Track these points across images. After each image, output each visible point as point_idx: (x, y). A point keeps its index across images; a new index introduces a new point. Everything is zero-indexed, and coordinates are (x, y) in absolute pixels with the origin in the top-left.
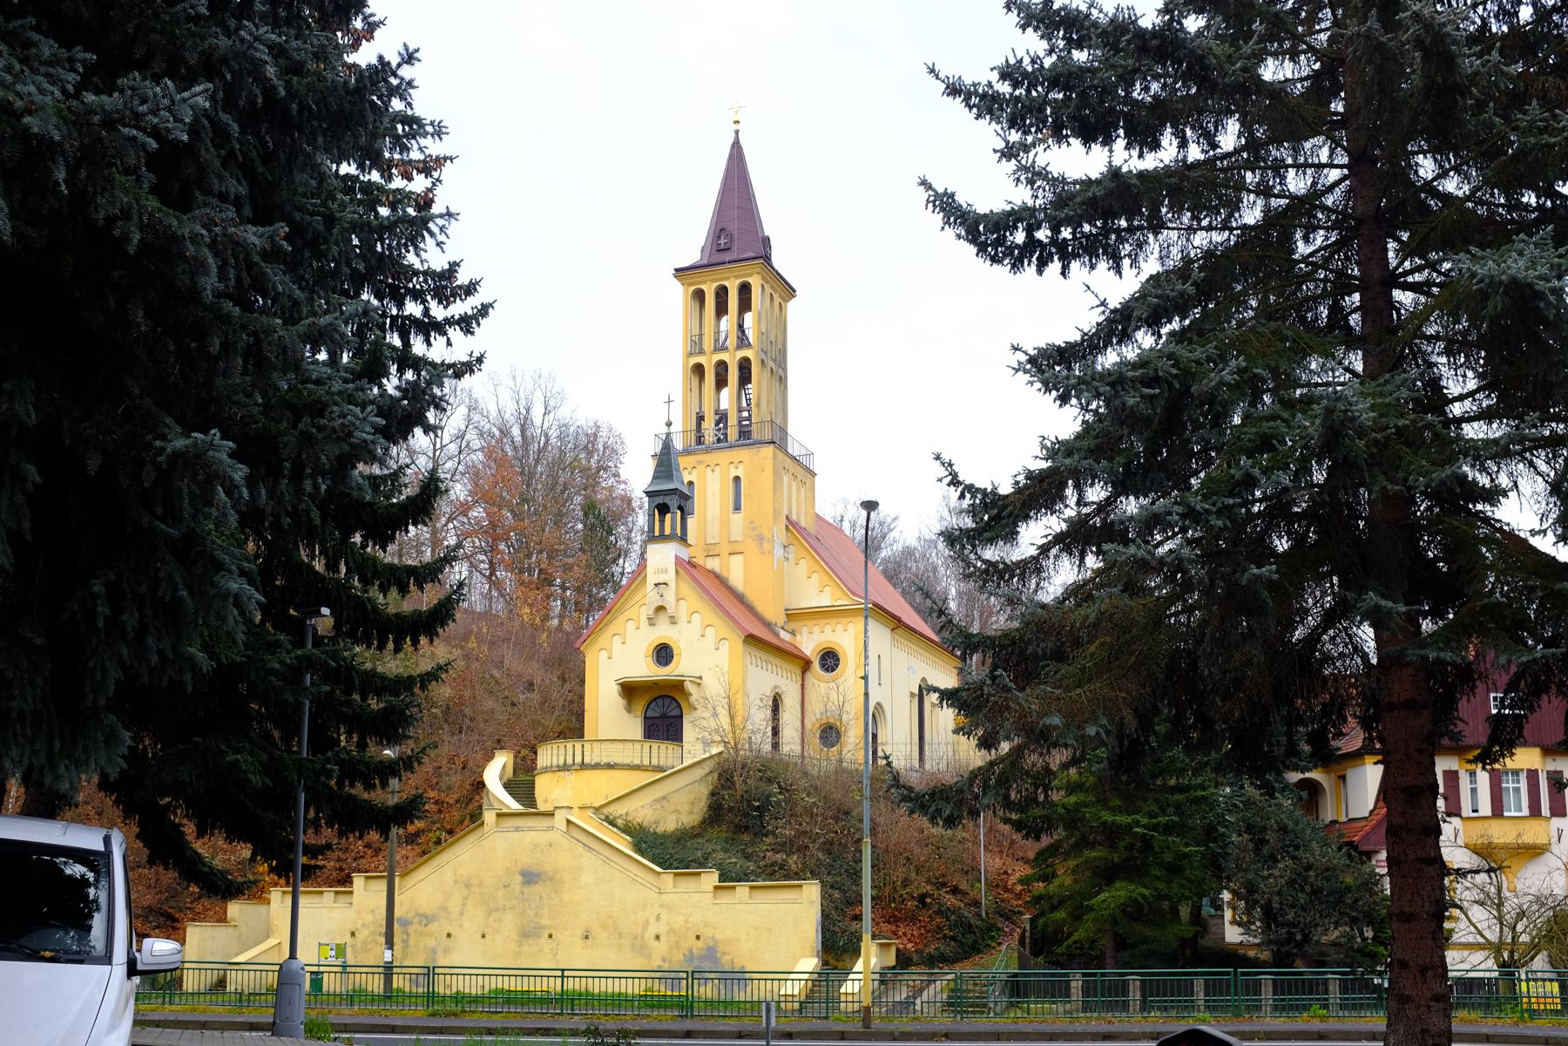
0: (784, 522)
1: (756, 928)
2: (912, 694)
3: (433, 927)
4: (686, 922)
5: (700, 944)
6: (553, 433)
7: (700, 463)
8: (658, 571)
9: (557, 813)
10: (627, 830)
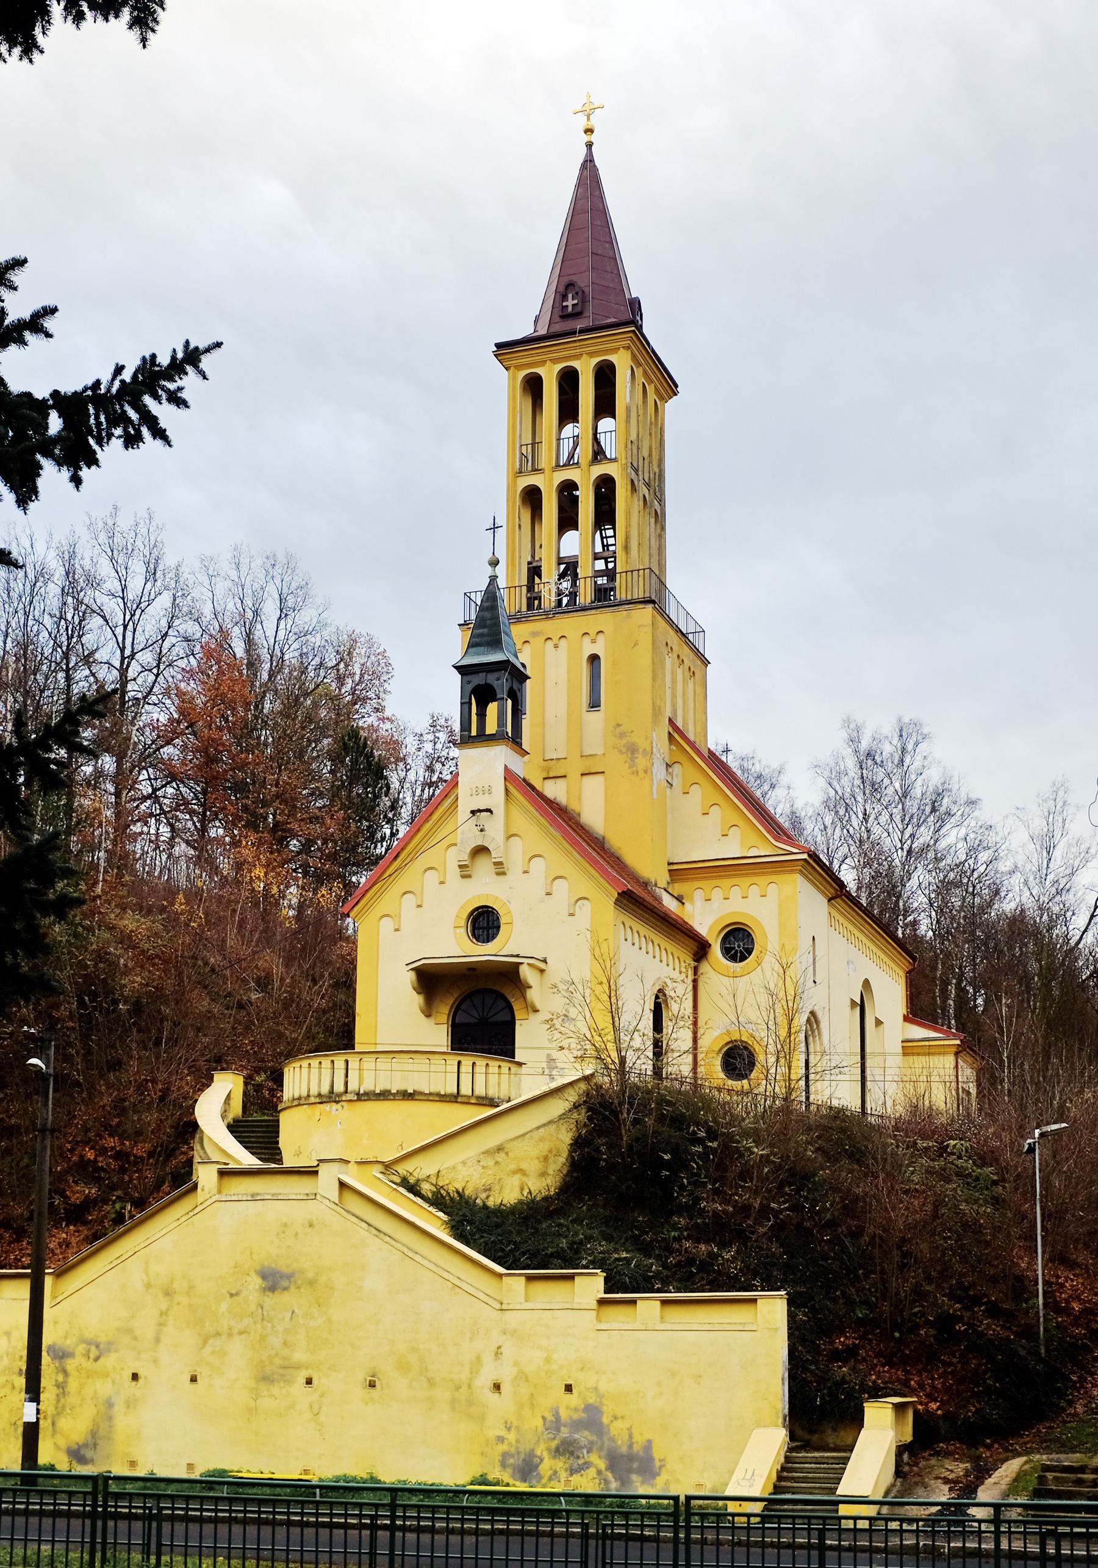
0: (666, 728)
1: (673, 1374)
2: (853, 1002)
3: (109, 1361)
4: (548, 1360)
5: (573, 1399)
6: (291, 656)
7: (535, 634)
8: (477, 792)
9: (323, 1169)
10: (438, 1201)
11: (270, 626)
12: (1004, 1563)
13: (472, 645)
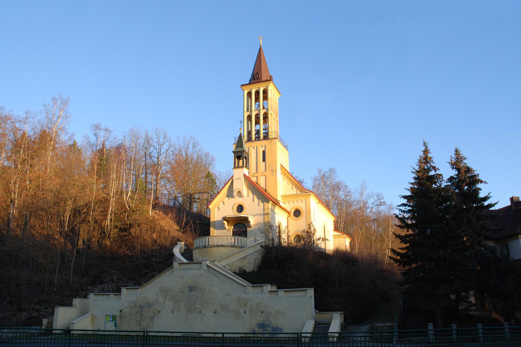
0: (280, 166)
7: (250, 146)
11: (191, 149)
12: (148, 346)
13: (236, 147)
